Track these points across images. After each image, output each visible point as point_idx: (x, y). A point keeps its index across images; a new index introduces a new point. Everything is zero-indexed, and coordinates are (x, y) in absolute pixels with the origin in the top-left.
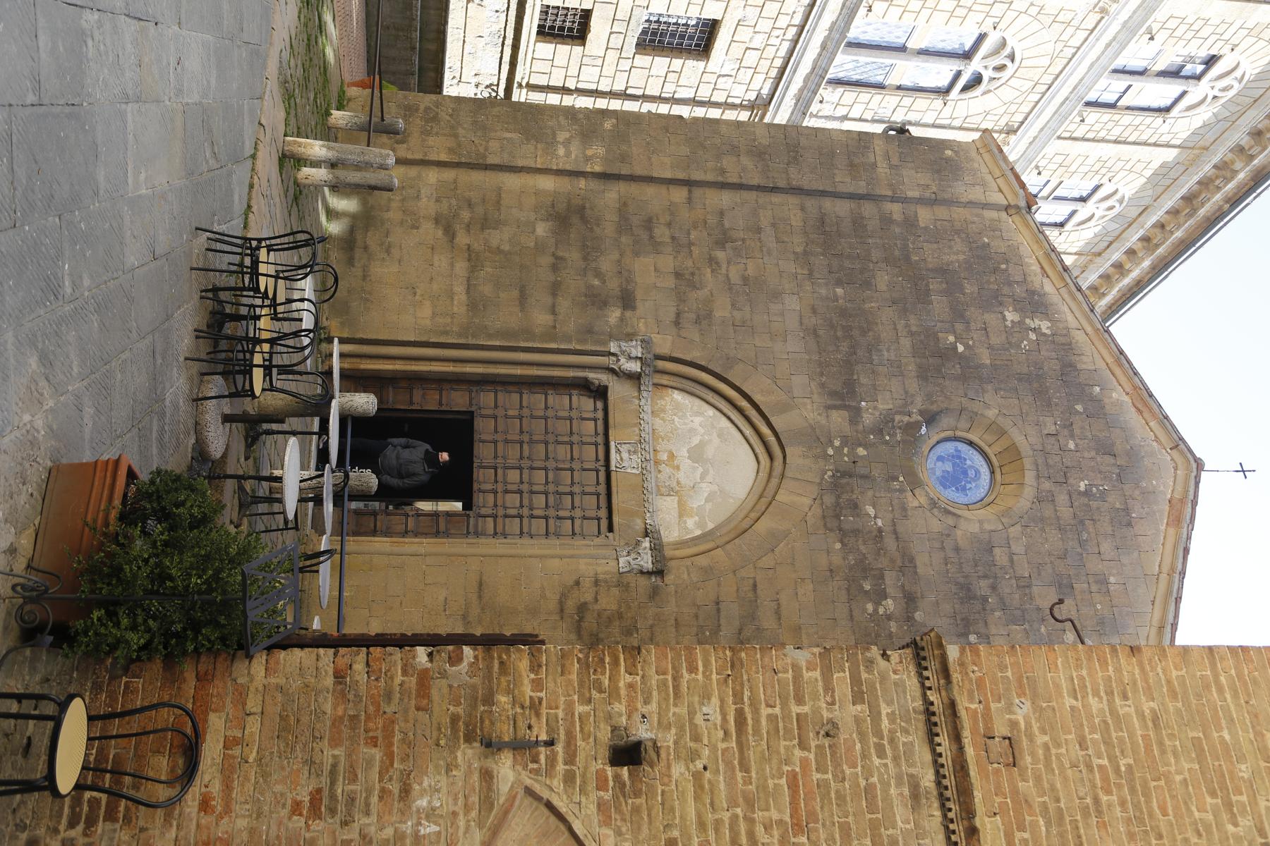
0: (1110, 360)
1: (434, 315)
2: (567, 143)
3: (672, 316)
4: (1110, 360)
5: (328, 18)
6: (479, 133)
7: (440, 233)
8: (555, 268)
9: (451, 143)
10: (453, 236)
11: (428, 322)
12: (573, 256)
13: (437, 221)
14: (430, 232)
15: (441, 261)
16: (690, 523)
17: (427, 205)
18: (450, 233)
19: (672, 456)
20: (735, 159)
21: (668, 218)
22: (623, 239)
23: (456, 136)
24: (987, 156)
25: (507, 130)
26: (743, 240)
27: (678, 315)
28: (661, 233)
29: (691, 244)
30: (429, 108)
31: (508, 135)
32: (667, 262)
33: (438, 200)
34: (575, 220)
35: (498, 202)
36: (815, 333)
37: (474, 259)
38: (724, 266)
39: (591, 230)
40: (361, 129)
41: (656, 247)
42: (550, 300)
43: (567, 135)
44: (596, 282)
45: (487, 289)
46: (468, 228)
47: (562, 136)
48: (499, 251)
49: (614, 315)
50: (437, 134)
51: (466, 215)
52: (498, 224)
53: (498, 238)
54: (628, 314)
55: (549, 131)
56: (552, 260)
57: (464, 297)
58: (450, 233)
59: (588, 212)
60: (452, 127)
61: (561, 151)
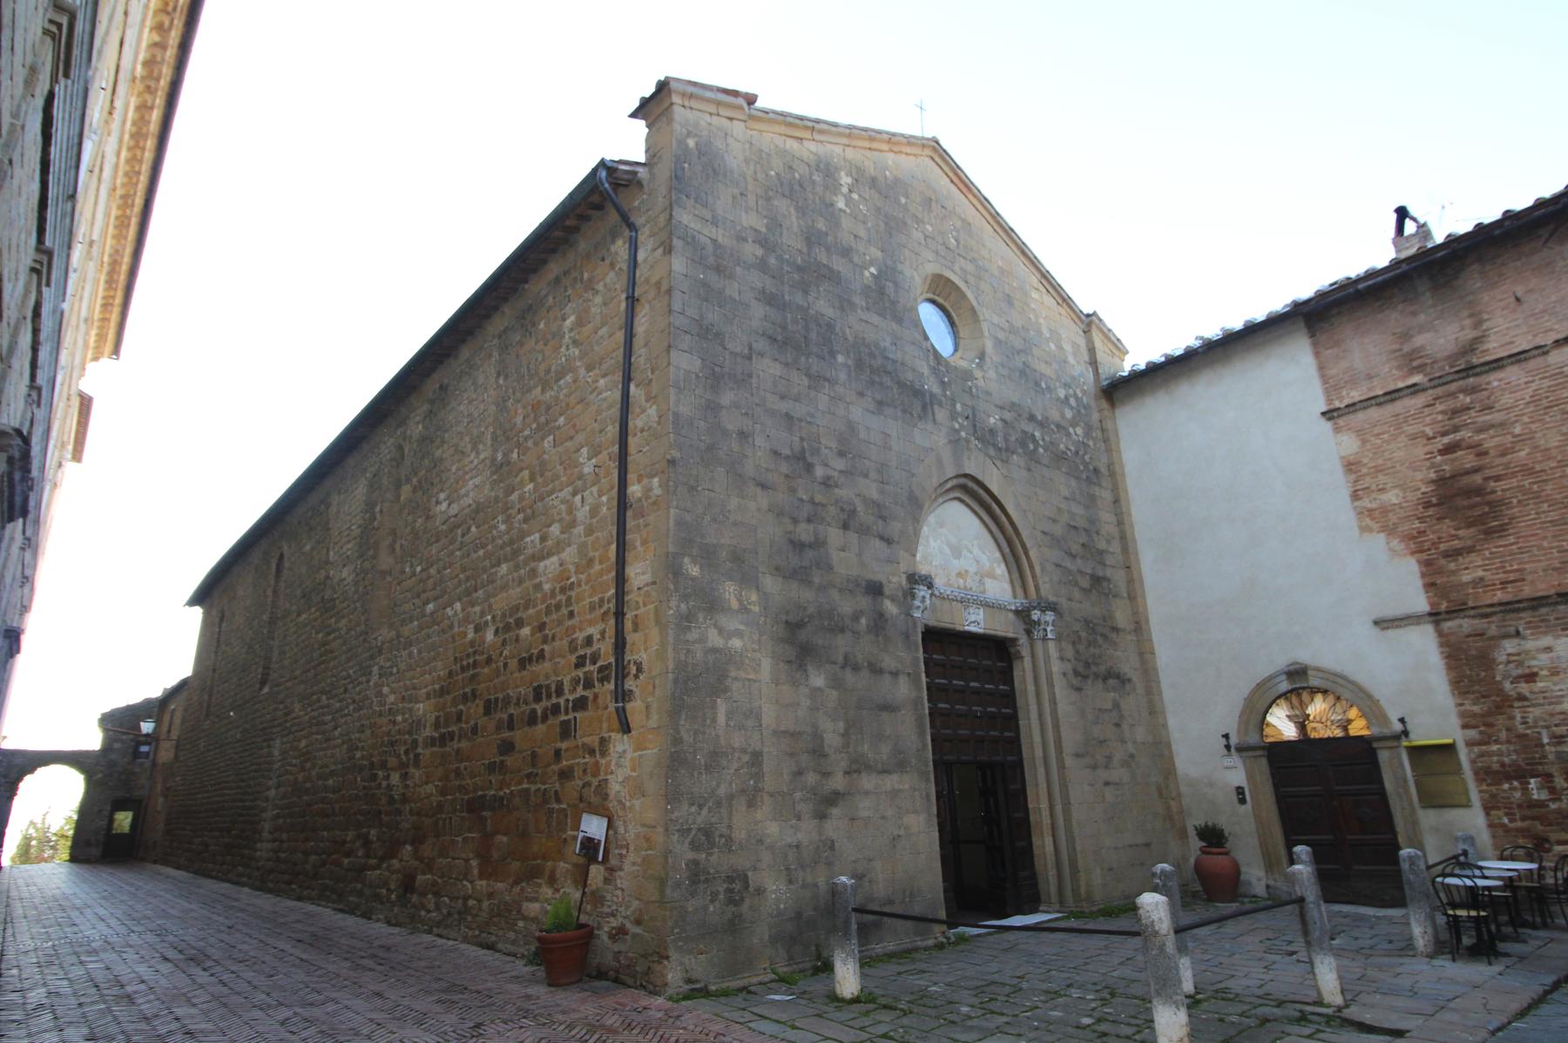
0: (867, 144)
1: (915, 812)
3: (883, 545)
4: (867, 144)
6: (724, 763)
7: (835, 811)
8: (856, 668)
9: (740, 806)
10: (837, 793)
12: (842, 643)
13: (822, 816)
14: (835, 826)
15: (865, 807)
17: (806, 832)
18: (833, 799)
19: (959, 575)
20: (724, 412)
21: (787, 520)
22: (817, 580)
23: (731, 797)
24: (694, 104)
25: (714, 720)
26: (802, 439)
27: (882, 538)
28: (804, 532)
29: (812, 501)
30: (692, 843)
31: (721, 718)
32: (834, 535)
34: (803, 635)
35: (792, 734)
36: (880, 403)
37: (857, 767)
38: (830, 472)
39: (811, 616)
40: (1430, 614)
41: (819, 543)
42: (887, 678)
44: (863, 621)
45: (885, 750)
46: (826, 775)
47: (714, 639)
48: (846, 735)
49: (890, 608)
50: (730, 827)
51: (811, 778)
52: (817, 736)
53: (832, 739)
54: (887, 591)
55: (711, 658)
56: (848, 671)
57: (895, 777)
58: (833, 799)
59: (791, 618)
60: (719, 804)
61: (736, 643)
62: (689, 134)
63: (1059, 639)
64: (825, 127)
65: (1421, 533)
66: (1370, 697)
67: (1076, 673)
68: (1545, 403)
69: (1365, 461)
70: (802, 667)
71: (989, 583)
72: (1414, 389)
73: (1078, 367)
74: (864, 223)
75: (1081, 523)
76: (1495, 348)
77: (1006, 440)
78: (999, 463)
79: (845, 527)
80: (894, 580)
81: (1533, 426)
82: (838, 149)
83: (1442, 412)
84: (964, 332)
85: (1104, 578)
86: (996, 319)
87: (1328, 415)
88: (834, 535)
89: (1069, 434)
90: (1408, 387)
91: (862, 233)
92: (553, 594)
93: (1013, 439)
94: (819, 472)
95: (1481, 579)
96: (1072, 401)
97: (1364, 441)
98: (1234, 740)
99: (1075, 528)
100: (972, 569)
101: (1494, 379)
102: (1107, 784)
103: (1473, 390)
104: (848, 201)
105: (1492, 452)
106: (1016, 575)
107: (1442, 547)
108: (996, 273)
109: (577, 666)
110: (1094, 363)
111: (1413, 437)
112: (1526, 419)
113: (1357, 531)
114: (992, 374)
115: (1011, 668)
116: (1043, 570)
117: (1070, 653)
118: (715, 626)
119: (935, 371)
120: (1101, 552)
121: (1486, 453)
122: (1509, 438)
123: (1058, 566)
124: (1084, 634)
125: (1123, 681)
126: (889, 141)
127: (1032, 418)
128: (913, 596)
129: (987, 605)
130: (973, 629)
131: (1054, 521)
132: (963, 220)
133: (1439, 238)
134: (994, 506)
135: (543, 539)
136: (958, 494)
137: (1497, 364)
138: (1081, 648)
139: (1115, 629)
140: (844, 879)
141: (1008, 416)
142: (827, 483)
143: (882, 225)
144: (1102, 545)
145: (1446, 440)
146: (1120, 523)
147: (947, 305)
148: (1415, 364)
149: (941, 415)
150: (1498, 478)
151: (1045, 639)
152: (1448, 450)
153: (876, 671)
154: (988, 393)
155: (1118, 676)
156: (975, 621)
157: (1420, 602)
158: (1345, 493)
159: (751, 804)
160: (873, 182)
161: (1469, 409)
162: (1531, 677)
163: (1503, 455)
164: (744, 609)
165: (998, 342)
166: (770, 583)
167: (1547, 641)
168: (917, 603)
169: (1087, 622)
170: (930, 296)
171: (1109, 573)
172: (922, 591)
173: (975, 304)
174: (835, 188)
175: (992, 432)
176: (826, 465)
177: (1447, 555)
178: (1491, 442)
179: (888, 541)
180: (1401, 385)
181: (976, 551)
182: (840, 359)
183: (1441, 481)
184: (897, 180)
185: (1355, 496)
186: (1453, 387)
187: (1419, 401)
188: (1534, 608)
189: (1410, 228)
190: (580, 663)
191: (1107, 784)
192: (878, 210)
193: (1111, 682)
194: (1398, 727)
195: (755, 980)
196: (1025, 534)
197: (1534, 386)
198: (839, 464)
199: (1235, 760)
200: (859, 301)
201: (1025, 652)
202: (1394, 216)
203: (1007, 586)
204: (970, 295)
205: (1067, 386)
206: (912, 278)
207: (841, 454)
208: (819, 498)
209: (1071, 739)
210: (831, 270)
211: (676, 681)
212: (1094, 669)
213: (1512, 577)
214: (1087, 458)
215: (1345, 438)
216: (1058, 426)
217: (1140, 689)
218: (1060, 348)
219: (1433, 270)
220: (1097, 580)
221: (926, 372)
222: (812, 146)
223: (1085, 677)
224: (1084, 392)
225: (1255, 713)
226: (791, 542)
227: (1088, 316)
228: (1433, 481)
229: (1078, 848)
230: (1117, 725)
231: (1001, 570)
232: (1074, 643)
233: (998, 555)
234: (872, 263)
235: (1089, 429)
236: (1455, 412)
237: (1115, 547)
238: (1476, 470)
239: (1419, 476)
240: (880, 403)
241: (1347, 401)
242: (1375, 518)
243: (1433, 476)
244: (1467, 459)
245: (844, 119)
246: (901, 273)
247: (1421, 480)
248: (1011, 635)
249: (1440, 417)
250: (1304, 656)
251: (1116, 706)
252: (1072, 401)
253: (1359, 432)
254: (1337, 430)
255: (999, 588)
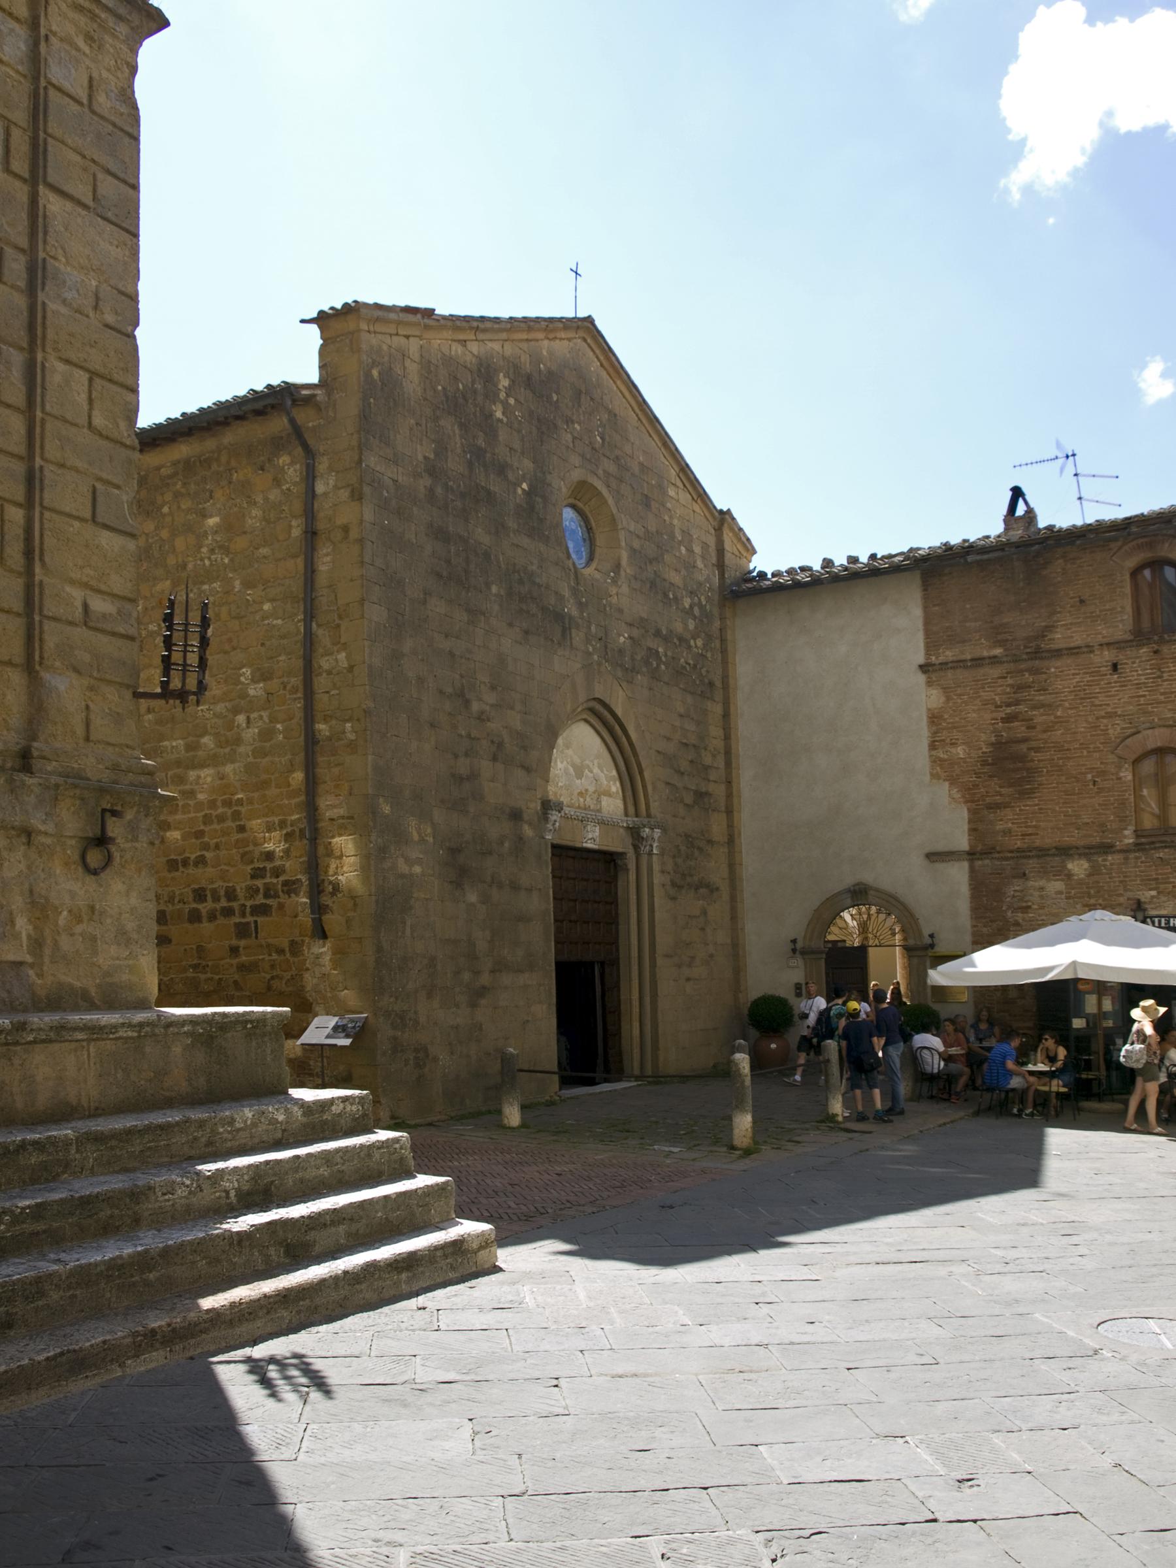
2: (410, 862)
5: (1002, 961)
7: (483, 1002)
8: (500, 886)
10: (484, 987)
11: (545, 1007)
13: (473, 1005)
16: (614, 789)
19: (581, 794)
24: (379, 327)
26: (462, 676)
27: (523, 767)
28: (463, 766)
29: (469, 736)
32: (485, 767)
33: (457, 1006)
36: (527, 632)
37: (500, 967)
41: (473, 776)
43: (401, 861)
44: (507, 845)
46: (477, 973)
47: (403, 867)
49: (528, 831)
50: (415, 1012)
51: (466, 976)
54: (526, 817)
58: (482, 992)
61: (417, 869)
62: (374, 364)
63: (662, 853)
64: (488, 325)
65: (976, 786)
66: (912, 915)
67: (674, 884)
68: (1082, 694)
69: (946, 716)
70: (458, 884)
71: (605, 802)
72: (994, 660)
73: (705, 572)
74: (519, 431)
75: (693, 739)
76: (1059, 639)
77: (633, 659)
78: (624, 684)
79: (495, 759)
80: (532, 805)
81: (1070, 712)
82: (496, 346)
83: (1012, 686)
84: (600, 540)
85: (707, 794)
86: (632, 527)
87: (924, 668)
88: (485, 767)
89: (690, 647)
90: (990, 658)
91: (517, 445)
92: (212, 804)
93: (639, 657)
94: (475, 707)
95: (1010, 831)
96: (696, 611)
97: (948, 699)
98: (799, 945)
99: (686, 745)
100: (591, 789)
101: (1054, 666)
102: (688, 979)
103: (1035, 671)
104: (505, 405)
105: (1039, 728)
106: (629, 793)
107: (988, 800)
108: (636, 470)
109: (253, 877)
110: (721, 565)
111: (986, 703)
112: (1067, 704)
113: (928, 778)
114: (625, 589)
115: (615, 878)
116: (654, 788)
117: (670, 867)
118: (402, 856)
119: (575, 592)
120: (707, 768)
121: (1034, 727)
122: (1052, 718)
123: (668, 784)
124: (683, 848)
125: (712, 889)
126: (546, 329)
127: (658, 633)
128: (546, 820)
129: (602, 823)
130: (589, 845)
131: (668, 739)
132: (610, 412)
133: (1042, 523)
134: (617, 728)
135: (189, 748)
136: (585, 716)
137: (1058, 653)
138: (680, 861)
139: (710, 842)
140: (511, 1050)
141: (636, 633)
142: (482, 718)
143: (534, 430)
144: (708, 760)
145: (1009, 710)
146: (727, 737)
147: (586, 509)
148: (999, 637)
149: (578, 637)
150: (1037, 750)
151: (650, 854)
152: (1009, 719)
153: (515, 887)
154: (621, 611)
155: (708, 886)
156: (592, 838)
157: (962, 842)
158: (925, 743)
159: (430, 996)
160: (528, 381)
161: (1030, 687)
162: (1026, 909)
163: (1045, 731)
164: (422, 840)
165: (633, 552)
166: (438, 815)
167: (1042, 883)
168: (550, 826)
169: (687, 836)
170: (571, 501)
171: (711, 787)
172: (554, 816)
173: (615, 511)
174: (491, 395)
175: (621, 651)
176: (481, 700)
177: (990, 807)
178: (1040, 718)
179: (528, 770)
180: (985, 654)
181: (596, 770)
182: (494, 589)
183: (999, 745)
184: (550, 373)
185: (933, 746)
186: (1023, 666)
187: (994, 672)
188: (1038, 857)
189: (1021, 510)
190: (258, 874)
191: (688, 979)
192: (531, 413)
193: (702, 891)
194: (928, 941)
195: (435, 1119)
196: (642, 754)
197: (1078, 678)
198: (491, 698)
199: (798, 961)
200: (511, 523)
201: (632, 866)
202: (1010, 494)
203: (619, 803)
204: (610, 501)
205: (692, 593)
206: (560, 489)
207: (493, 688)
208: (474, 733)
209: (664, 941)
210: (489, 492)
211: (377, 902)
212: (689, 879)
213: (1030, 831)
214: (704, 671)
215: (935, 692)
216: (681, 639)
217: (725, 896)
218: (690, 551)
219: (1026, 556)
220: (700, 795)
221: (567, 593)
222: (474, 347)
223: (680, 887)
224: (708, 599)
225: (828, 912)
226: (453, 775)
227: (721, 512)
228: (992, 744)
229: (660, 1032)
230: (703, 929)
231: (615, 787)
232: (674, 857)
233: (614, 773)
234: (524, 479)
235: (709, 638)
236: (1019, 688)
237: (720, 762)
238: (1025, 740)
239: (983, 737)
240: (527, 632)
241: (942, 659)
242: (943, 769)
243: (993, 739)
244: (1019, 729)
245: (504, 311)
246: (549, 485)
247: (985, 739)
248: (620, 850)
249: (1008, 690)
250: (868, 878)
251: (704, 913)
252: (696, 611)
253: (945, 689)
254: (929, 683)
255: (613, 806)
